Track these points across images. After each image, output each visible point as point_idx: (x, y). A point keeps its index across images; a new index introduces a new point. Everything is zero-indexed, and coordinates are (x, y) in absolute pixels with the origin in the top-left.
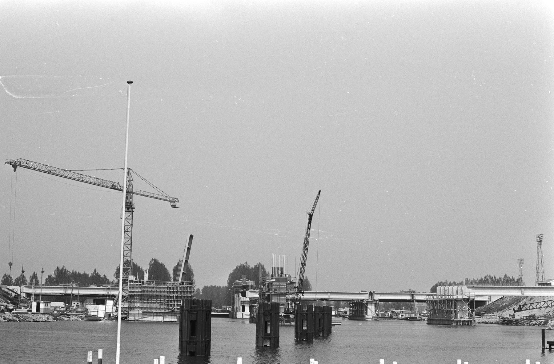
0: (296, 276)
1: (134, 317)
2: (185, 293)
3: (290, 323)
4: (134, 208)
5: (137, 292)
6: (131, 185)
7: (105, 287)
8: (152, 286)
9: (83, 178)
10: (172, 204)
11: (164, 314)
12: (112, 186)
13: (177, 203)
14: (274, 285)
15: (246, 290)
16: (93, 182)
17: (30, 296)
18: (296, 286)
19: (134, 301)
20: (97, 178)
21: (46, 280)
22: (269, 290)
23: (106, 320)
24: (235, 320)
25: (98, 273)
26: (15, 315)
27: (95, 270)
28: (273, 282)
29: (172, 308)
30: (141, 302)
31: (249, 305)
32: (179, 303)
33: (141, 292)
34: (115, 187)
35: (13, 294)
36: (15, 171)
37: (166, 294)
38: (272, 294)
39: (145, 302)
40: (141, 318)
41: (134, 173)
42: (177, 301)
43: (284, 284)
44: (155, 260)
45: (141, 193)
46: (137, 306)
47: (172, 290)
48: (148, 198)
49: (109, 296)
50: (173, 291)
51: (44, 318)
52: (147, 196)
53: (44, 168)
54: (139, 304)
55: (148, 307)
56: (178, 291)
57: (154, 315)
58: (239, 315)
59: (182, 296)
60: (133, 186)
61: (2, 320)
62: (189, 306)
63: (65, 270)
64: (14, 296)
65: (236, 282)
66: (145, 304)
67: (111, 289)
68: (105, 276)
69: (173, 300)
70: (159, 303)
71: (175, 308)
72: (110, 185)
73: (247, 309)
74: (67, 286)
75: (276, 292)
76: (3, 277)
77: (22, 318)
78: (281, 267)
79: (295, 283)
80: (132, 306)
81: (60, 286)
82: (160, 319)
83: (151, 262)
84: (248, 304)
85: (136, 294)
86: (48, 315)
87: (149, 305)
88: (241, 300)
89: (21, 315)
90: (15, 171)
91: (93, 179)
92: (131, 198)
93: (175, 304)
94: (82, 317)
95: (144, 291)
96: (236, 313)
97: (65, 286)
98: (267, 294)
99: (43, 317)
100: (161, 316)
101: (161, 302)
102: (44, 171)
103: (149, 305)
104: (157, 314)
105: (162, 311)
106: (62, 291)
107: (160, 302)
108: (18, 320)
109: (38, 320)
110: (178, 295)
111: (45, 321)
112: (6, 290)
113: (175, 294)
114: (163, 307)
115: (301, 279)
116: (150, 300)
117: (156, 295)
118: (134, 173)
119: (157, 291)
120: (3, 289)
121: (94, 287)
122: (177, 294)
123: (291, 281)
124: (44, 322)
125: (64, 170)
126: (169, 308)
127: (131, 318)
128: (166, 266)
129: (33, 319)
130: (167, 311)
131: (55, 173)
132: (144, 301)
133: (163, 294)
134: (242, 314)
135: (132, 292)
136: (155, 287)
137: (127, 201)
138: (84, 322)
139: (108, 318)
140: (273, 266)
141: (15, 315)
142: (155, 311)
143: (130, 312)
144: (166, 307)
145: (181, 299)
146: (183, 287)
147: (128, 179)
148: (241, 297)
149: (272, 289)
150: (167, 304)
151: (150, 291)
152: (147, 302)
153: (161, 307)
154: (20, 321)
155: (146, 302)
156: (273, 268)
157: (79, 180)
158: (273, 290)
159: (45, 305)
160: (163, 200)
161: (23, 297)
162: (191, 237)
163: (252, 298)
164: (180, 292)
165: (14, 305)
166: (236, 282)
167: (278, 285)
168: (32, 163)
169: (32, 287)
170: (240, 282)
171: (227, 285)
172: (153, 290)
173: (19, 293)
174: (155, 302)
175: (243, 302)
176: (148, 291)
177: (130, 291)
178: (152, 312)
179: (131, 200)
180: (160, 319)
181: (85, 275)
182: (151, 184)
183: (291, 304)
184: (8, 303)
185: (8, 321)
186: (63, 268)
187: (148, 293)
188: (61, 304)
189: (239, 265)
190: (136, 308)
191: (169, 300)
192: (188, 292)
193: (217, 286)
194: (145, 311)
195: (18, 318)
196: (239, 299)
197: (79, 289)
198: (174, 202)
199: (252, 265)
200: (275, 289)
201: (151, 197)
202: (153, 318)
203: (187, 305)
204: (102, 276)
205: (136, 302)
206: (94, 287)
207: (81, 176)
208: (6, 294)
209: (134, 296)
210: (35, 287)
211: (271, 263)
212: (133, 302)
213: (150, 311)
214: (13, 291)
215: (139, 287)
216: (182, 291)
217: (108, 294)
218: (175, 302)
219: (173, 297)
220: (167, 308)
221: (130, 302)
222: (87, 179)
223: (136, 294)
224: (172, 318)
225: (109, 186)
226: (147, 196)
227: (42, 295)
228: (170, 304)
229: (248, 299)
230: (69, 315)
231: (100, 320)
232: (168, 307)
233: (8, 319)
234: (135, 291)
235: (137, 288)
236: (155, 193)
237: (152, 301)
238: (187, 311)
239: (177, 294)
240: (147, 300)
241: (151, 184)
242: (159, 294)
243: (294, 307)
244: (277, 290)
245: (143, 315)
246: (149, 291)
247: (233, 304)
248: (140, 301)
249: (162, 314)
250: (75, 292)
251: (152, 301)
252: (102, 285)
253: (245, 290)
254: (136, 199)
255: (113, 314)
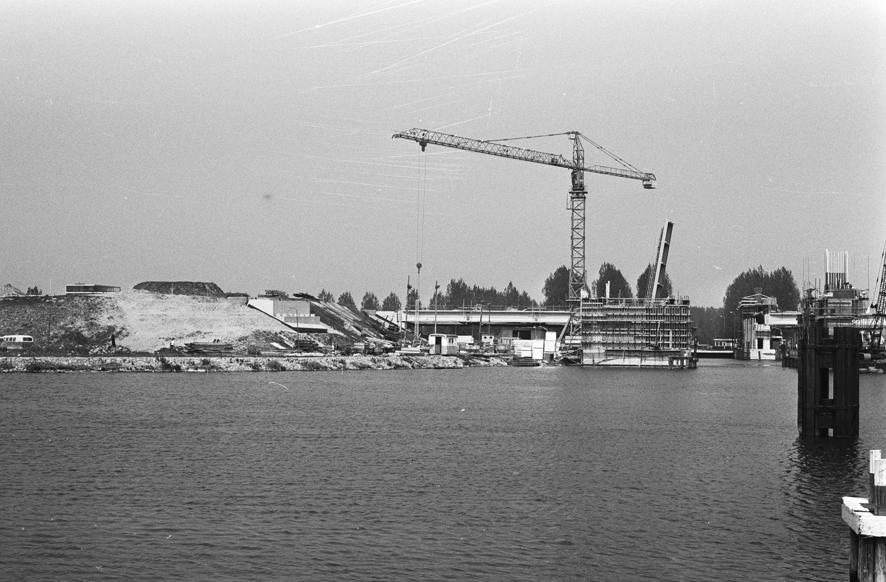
0: (817, 285)
1: (592, 360)
2: (676, 318)
3: (867, 367)
4: (587, 193)
5: (596, 318)
6: (581, 157)
7: (531, 310)
8: (620, 306)
9: (507, 151)
10: (645, 183)
11: (642, 354)
12: (552, 161)
13: (653, 181)
14: (830, 303)
15: (765, 313)
16: (523, 156)
17: (412, 327)
18: (874, 305)
19: (591, 332)
20: (529, 150)
21: (432, 301)
22: (821, 312)
23: (547, 364)
24: (748, 363)
25: (515, 289)
26: (405, 357)
27: (511, 284)
28: (828, 297)
29: (655, 343)
30: (603, 334)
31: (769, 338)
32: (667, 336)
33: (602, 318)
34: (557, 162)
35: (387, 325)
36: (423, 150)
37: (645, 320)
38: (827, 318)
39: (609, 334)
40: (604, 360)
41: (585, 138)
42: (664, 331)
43: (848, 301)
44: (608, 265)
45: (597, 169)
46: (597, 341)
47: (655, 314)
48: (629, 179)
49: (537, 324)
50: (657, 315)
51: (450, 362)
52: (607, 173)
53: (449, 140)
54: (599, 337)
55: (615, 342)
56: (664, 316)
57: (625, 356)
58: (754, 354)
59: (671, 324)
60: (583, 159)
61: (386, 366)
62: (818, 339)
63: (464, 284)
64: (388, 327)
65: (746, 300)
66: (610, 338)
67: (541, 313)
68: (525, 294)
69: (657, 331)
70: (632, 335)
71: (659, 344)
72: (548, 160)
73: (767, 343)
74: (470, 309)
75: (835, 315)
76: (364, 298)
77: (416, 363)
78: (842, 271)
79: (867, 299)
80: (588, 341)
81: (459, 311)
82: (635, 361)
83: (601, 269)
84: (768, 336)
85: (594, 320)
86: (455, 358)
87: (616, 340)
88: (756, 329)
89: (414, 358)
90: (423, 150)
91: (523, 151)
92: (582, 178)
93: (659, 337)
94: (508, 359)
95: (608, 316)
96: (748, 350)
97: (467, 309)
98: (818, 318)
99: (449, 360)
100: (636, 356)
101: (637, 333)
102: (450, 145)
103: (616, 340)
104: (630, 354)
105: (639, 348)
106: (462, 319)
107: (635, 334)
108: (410, 366)
109: (441, 366)
110: (665, 322)
111: (454, 368)
112: (376, 318)
113: (660, 321)
114: (640, 342)
115: (883, 293)
116: (618, 331)
117: (629, 322)
118: (585, 138)
119: (628, 316)
120: (370, 316)
121: (513, 310)
122: (663, 320)
123: (860, 297)
124: (451, 368)
125: (479, 141)
126: (650, 343)
127: (587, 361)
128: (624, 275)
129: (434, 365)
130: (647, 349)
131: (466, 146)
132: (608, 333)
133: (639, 320)
134: (759, 352)
135: (588, 318)
136: (626, 309)
137: (576, 182)
138: (512, 368)
139: (550, 361)
140: (828, 271)
141: (405, 357)
142: (626, 349)
143: (585, 351)
144: (644, 342)
145: (671, 328)
146: (673, 309)
147: (576, 149)
148: (757, 324)
149: (827, 310)
150: (647, 337)
151: (618, 316)
152: (613, 334)
153: (637, 342)
154: (413, 367)
155: (611, 334)
156: (827, 274)
157: (502, 155)
158: (829, 311)
159: (450, 342)
160: (632, 178)
161: (402, 329)
162: (670, 225)
163: (774, 326)
164: (668, 316)
165: (392, 342)
166: (746, 300)
167: (838, 303)
168: (431, 135)
169: (414, 312)
170: (753, 300)
171: (722, 305)
172: (623, 314)
173: (395, 322)
174: (626, 333)
175: (760, 332)
176: (614, 316)
177: (584, 315)
178: (622, 351)
179: (581, 180)
180: (635, 361)
181: (492, 292)
182: (610, 154)
183: (865, 335)
184: (381, 338)
185: (395, 368)
186: (460, 282)
187: (614, 320)
188: (469, 339)
189: (746, 272)
190: (594, 343)
191: (649, 331)
192: (681, 316)
193: (708, 308)
194: (610, 348)
195: (411, 362)
196: (752, 328)
197: (490, 314)
198: (649, 180)
199: (769, 270)
200: (833, 311)
201: (612, 174)
202: (624, 361)
203: (814, 339)
204: (521, 293)
205: (595, 334)
206: (513, 310)
207: (505, 148)
208: (375, 324)
209: (590, 324)
210: (420, 312)
211: (826, 268)
212: (590, 334)
213: (617, 348)
214: (386, 320)
215: (599, 310)
216: (671, 316)
217: (469, 321)
218: (659, 334)
219: (657, 326)
220: (647, 344)
221: (585, 334)
222: (514, 153)
223: (594, 320)
224: (655, 360)
225: (547, 161)
226: (607, 173)
227: (437, 325)
228: (652, 337)
229: (767, 328)
230: (487, 357)
231: (538, 365)
232: (648, 342)
233: (395, 364)
234: (592, 317)
235: (595, 310)
236: (618, 167)
237: (622, 333)
238: (813, 350)
239: (663, 320)
240: (613, 331)
241: (610, 154)
242: (632, 320)
243: (870, 341)
244: (837, 311)
245: (606, 355)
246: (616, 316)
247: (741, 336)
248: (601, 333)
249: (638, 354)
250: (485, 319)
251: (622, 333)
252: (526, 308)
253: (762, 312)
254: (589, 180)
255: (557, 355)
